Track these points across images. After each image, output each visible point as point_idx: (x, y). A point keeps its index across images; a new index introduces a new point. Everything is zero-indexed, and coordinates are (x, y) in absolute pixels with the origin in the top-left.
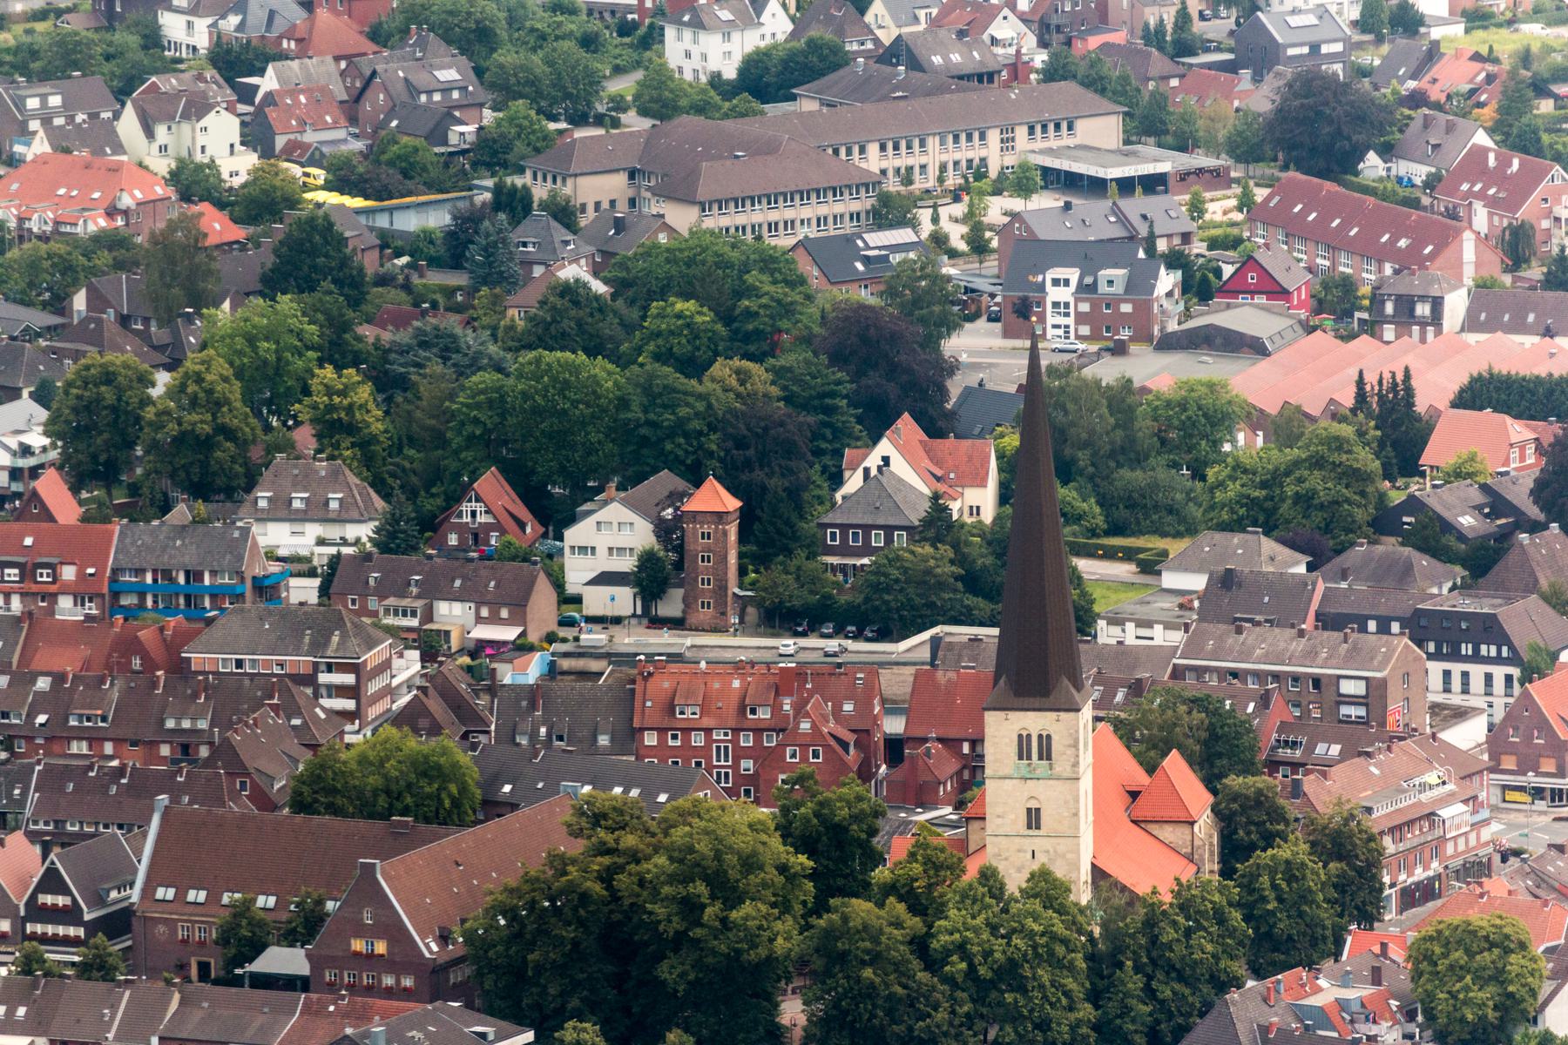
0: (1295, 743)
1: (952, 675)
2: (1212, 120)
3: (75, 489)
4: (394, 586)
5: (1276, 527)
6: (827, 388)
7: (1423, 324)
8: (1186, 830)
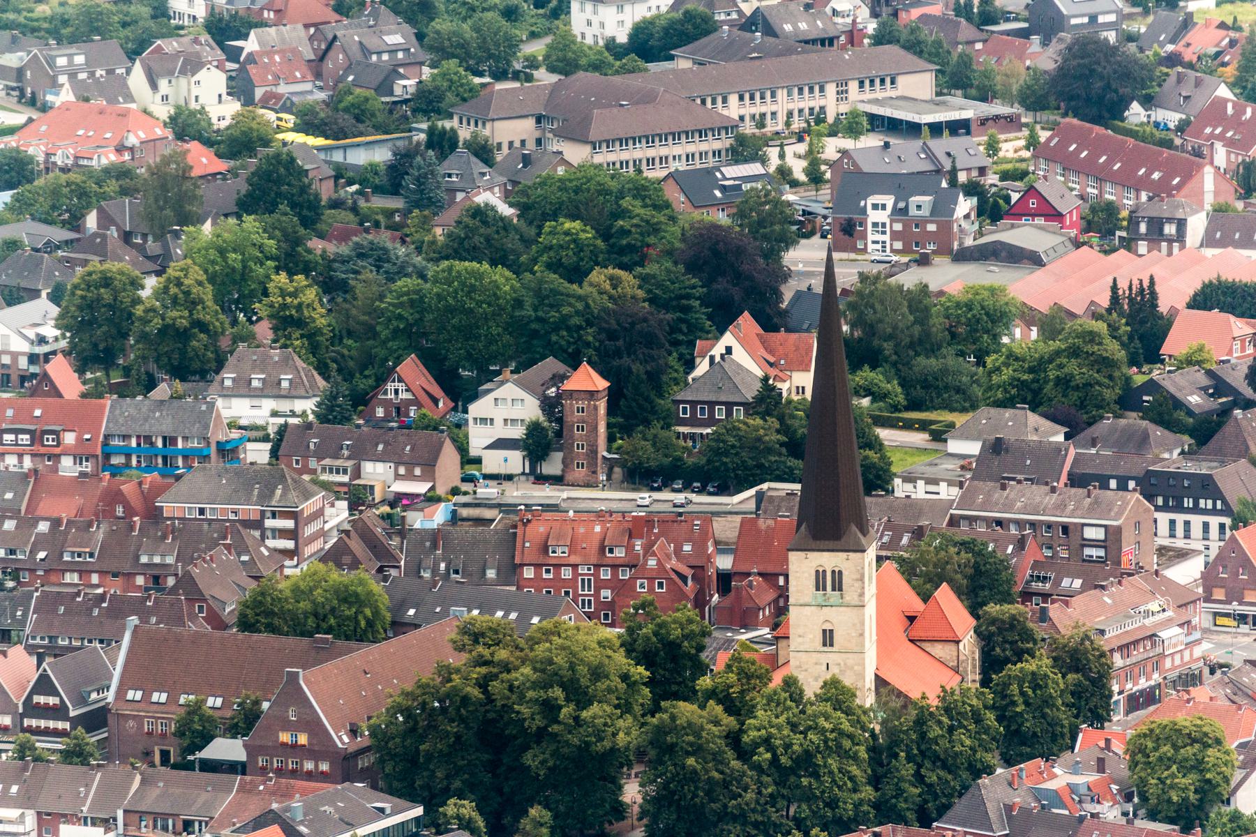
0: (1045, 578)
1: (771, 522)
2: (1007, 75)
3: (81, 371)
4: (329, 450)
5: (1041, 404)
6: (683, 292)
7: (1170, 241)
8: (952, 647)
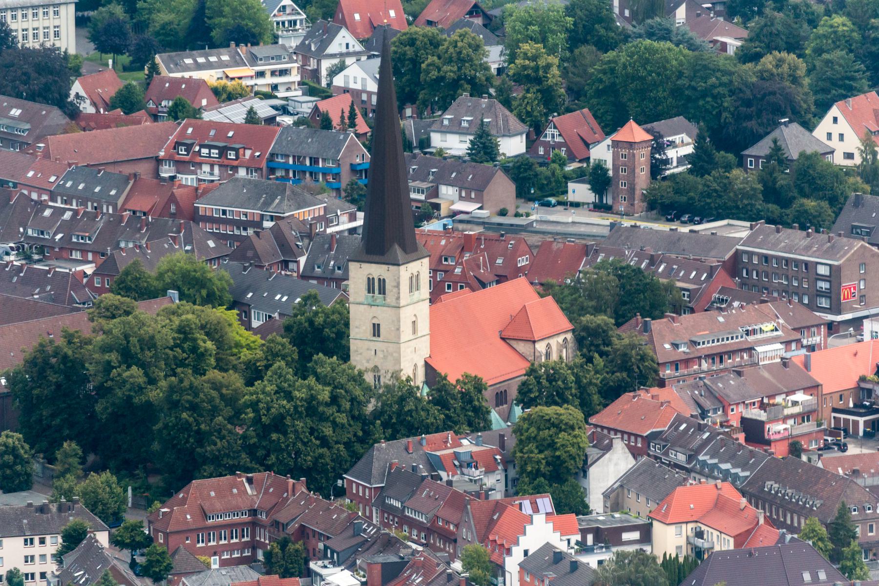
1: (561, 246)
6: (848, 74)
8: (530, 345)
